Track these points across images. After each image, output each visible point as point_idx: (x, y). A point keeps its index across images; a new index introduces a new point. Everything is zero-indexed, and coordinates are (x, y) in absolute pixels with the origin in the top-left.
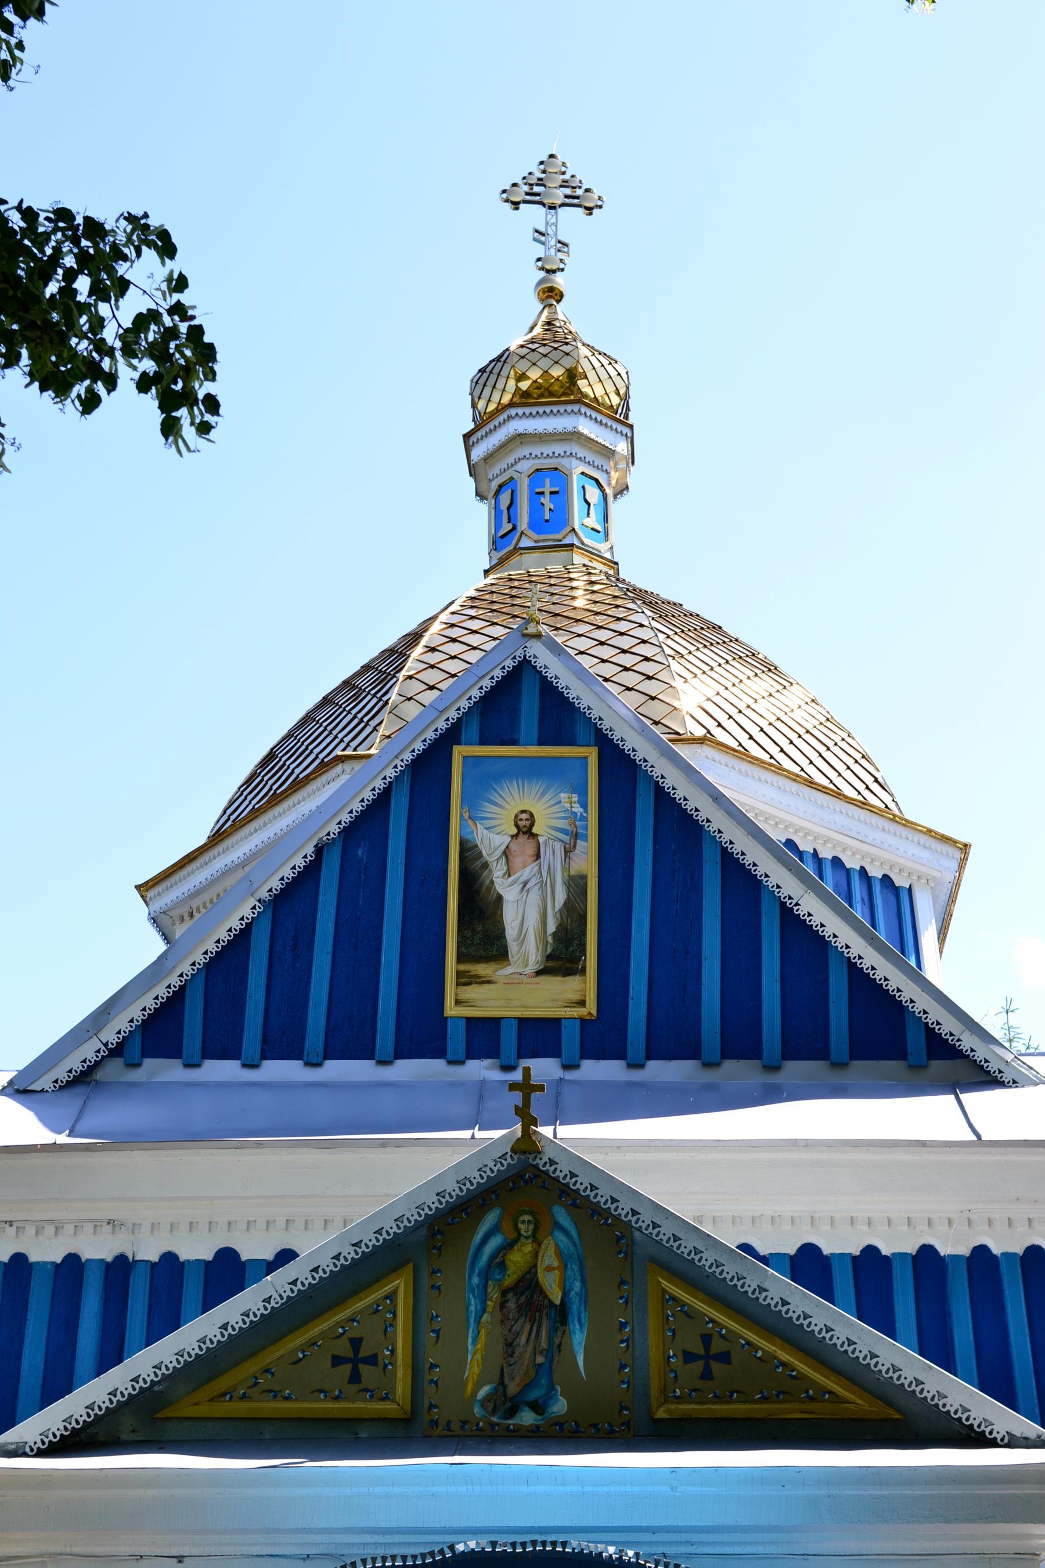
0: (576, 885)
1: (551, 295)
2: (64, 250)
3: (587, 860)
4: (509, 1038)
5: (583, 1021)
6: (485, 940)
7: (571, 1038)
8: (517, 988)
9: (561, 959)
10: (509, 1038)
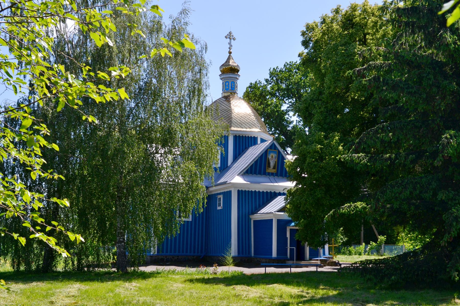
0: (275, 162)
1: (230, 53)
2: (179, 153)
3: (276, 160)
4: (270, 174)
5: (188, 222)
6: (269, 166)
7: (274, 174)
8: (271, 170)
9: (274, 168)
10: (270, 174)
